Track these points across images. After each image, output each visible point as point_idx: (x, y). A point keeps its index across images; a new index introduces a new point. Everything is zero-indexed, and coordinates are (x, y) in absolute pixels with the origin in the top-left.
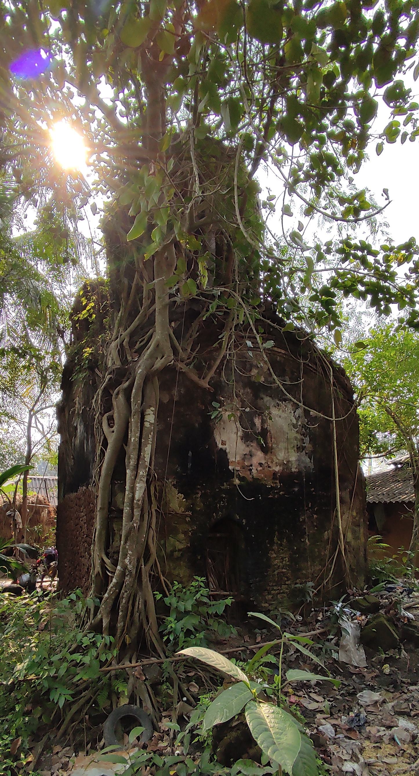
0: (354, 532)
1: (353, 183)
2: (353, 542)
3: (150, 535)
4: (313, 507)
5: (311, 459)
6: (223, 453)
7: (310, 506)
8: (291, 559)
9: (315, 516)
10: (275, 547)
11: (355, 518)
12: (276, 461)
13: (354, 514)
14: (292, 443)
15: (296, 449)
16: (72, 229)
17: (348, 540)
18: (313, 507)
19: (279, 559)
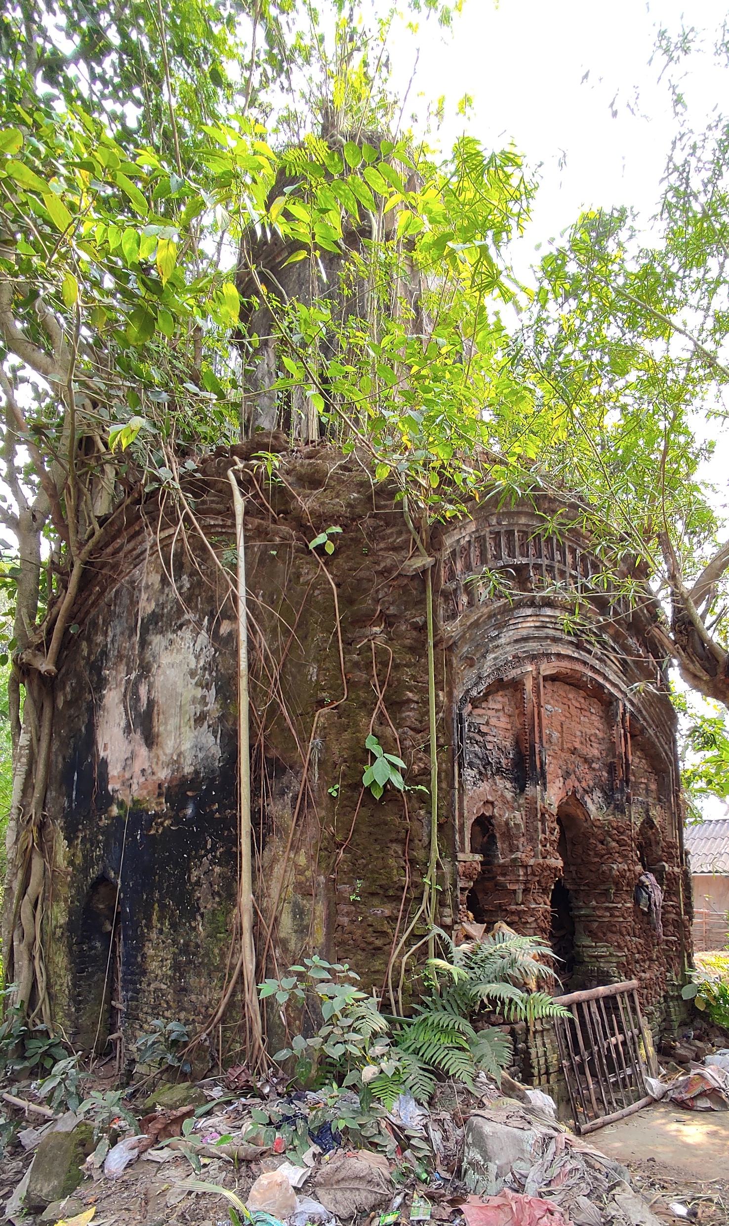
0: (299, 913)
1: (675, 98)
2: (293, 942)
3: (254, 1032)
4: (214, 849)
5: (216, 737)
6: (104, 763)
7: (209, 847)
8: (176, 966)
9: (217, 869)
10: (154, 935)
11: (301, 872)
12: (163, 758)
13: (302, 860)
14: (186, 712)
15: (192, 722)
16: (582, 817)
17: (282, 935)
18: (214, 849)
19: (158, 959)
